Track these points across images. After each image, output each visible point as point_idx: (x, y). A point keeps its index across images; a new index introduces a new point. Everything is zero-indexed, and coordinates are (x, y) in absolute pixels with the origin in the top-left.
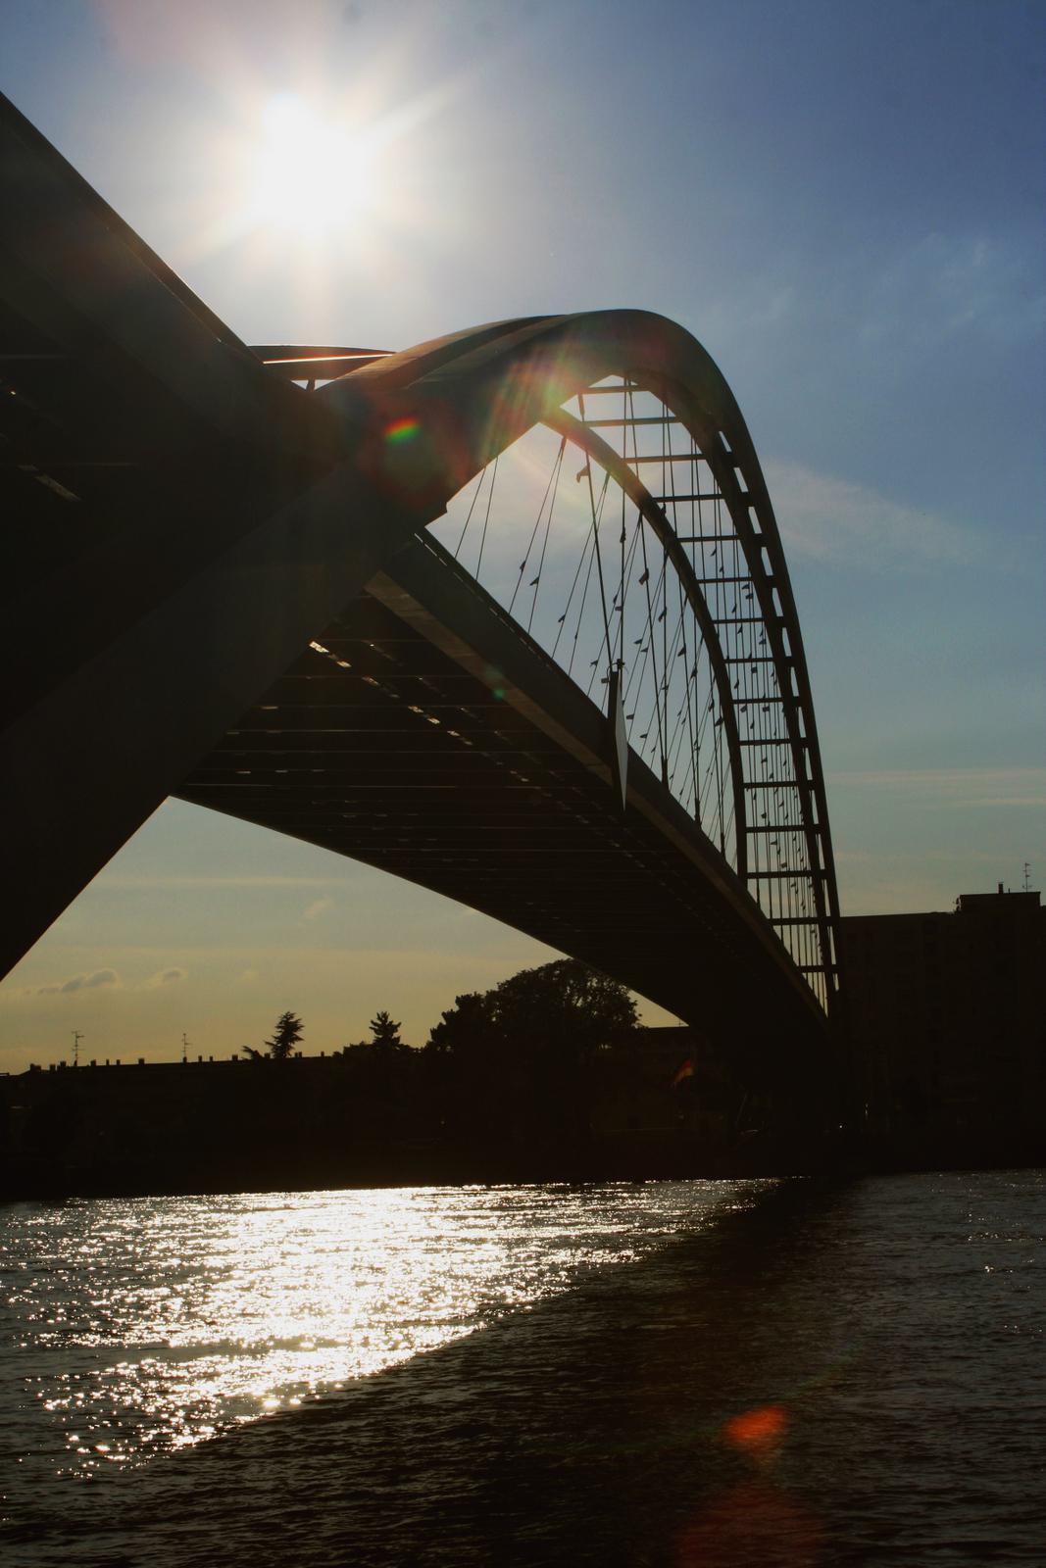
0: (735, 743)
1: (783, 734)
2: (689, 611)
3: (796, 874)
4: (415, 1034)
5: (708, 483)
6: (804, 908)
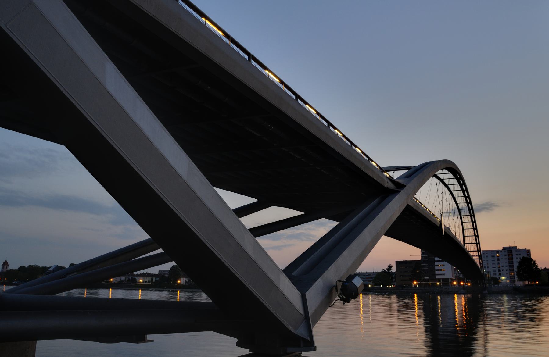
2: (450, 195)
4: (518, 248)
6: (470, 240)
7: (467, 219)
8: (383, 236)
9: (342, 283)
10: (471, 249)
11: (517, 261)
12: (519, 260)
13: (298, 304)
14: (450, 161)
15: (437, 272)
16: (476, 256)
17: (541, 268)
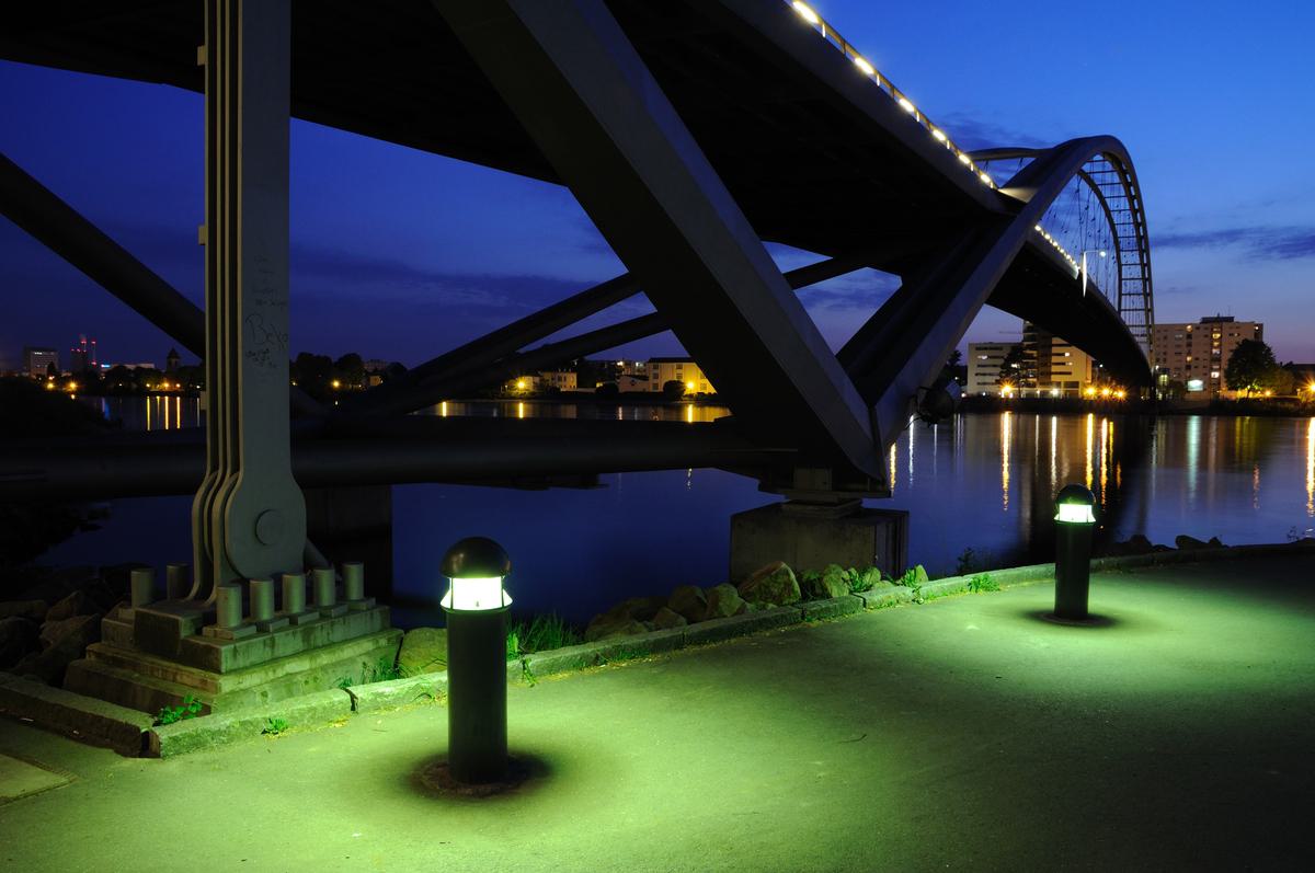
0: (1120, 266)
1: (1138, 262)
5: (1116, 179)
7: (1130, 257)
9: (925, 391)
12: (1234, 347)
14: (1109, 136)
15: (1054, 369)
16: (1142, 335)
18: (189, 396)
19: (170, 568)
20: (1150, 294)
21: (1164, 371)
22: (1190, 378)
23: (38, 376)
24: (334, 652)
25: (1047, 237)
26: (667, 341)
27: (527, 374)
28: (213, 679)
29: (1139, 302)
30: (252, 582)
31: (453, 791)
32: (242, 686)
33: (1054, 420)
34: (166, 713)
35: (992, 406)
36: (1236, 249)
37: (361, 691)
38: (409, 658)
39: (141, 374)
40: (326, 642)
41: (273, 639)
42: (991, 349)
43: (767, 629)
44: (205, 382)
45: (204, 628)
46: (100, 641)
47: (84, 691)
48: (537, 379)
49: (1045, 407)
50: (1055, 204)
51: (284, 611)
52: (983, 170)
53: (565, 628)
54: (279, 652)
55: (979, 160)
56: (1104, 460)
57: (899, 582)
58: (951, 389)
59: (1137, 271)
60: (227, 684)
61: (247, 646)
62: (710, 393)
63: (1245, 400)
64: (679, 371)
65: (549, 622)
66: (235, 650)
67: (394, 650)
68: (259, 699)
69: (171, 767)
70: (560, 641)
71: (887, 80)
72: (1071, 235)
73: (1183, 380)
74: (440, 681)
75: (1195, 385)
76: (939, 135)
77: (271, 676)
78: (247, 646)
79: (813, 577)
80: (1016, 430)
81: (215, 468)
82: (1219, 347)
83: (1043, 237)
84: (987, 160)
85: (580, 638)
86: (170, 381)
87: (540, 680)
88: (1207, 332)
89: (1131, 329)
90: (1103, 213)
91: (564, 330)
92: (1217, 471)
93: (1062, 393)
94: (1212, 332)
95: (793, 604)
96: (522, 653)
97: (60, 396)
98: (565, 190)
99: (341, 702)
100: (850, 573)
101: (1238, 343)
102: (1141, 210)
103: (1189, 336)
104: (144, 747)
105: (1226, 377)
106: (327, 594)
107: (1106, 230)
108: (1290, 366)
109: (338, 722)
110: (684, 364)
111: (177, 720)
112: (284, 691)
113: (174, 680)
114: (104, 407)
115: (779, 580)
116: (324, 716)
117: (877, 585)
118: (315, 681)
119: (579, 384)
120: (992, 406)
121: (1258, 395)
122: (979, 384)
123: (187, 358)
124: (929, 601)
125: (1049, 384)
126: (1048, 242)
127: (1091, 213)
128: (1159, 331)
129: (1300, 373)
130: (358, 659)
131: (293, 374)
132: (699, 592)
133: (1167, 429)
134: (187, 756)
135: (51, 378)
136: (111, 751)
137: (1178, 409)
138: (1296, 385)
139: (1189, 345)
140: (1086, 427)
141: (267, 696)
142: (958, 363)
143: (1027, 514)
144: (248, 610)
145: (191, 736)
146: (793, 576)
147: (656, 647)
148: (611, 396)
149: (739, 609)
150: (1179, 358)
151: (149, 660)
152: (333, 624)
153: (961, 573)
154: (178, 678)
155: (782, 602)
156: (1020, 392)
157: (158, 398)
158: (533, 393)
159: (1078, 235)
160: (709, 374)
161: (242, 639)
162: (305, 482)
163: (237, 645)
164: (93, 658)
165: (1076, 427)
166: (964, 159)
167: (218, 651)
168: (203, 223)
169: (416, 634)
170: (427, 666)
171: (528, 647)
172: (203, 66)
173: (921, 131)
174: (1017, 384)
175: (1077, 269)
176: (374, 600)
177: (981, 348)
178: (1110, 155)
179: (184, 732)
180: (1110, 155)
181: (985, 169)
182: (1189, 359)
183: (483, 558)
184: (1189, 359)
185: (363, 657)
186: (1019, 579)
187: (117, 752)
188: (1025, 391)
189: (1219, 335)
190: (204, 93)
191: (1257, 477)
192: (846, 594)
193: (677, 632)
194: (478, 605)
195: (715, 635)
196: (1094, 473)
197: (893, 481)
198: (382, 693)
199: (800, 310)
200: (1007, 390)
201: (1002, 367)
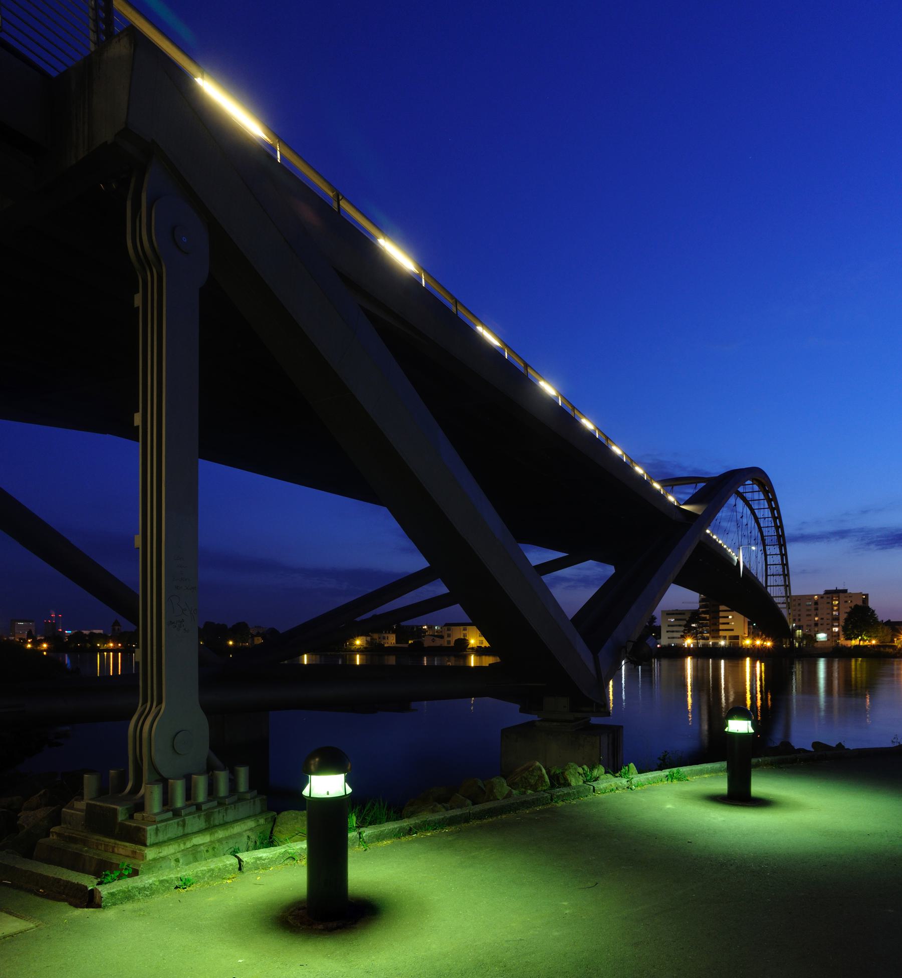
0: (766, 556)
1: (778, 553)
3: (780, 586)
5: (762, 497)
7: (773, 550)
8: (672, 584)
9: (632, 643)
10: (775, 594)
11: (846, 611)
12: (848, 610)
13: (591, 666)
16: (783, 603)
17: (882, 621)
18: (127, 652)
19: (112, 772)
20: (788, 575)
21: (799, 627)
22: (818, 632)
23: (20, 639)
24: (227, 829)
25: (715, 537)
26: (456, 611)
27: (361, 635)
28: (141, 850)
29: (780, 580)
30: (170, 781)
31: (310, 927)
32: (161, 855)
33: (723, 662)
34: (107, 875)
35: (680, 653)
36: (845, 544)
37: (246, 857)
38: (280, 832)
39: (93, 637)
40: (222, 822)
41: (184, 821)
42: (677, 614)
43: (528, 808)
44: (138, 642)
45: (135, 814)
46: (60, 824)
47: (49, 861)
48: (369, 638)
49: (716, 653)
50: (719, 514)
51: (192, 801)
52: (669, 493)
53: (389, 809)
54: (189, 830)
55: (667, 486)
56: (758, 689)
57: (617, 775)
58: (650, 642)
59: (778, 559)
60: (151, 854)
61: (166, 826)
62: (485, 647)
63: (856, 647)
64: (465, 632)
65: (377, 805)
66: (157, 830)
67: (269, 826)
68: (173, 863)
69: (109, 914)
70: (385, 818)
71: (604, 434)
72: (731, 536)
73: (813, 634)
74: (302, 848)
75: (822, 636)
76: (639, 470)
77: (182, 847)
78: (166, 826)
79: (558, 772)
80: (696, 669)
81: (145, 701)
82: (838, 610)
83: (712, 537)
84: (672, 486)
85: (399, 815)
86: (113, 642)
87: (371, 846)
88: (829, 600)
89: (775, 599)
90: (753, 521)
91: (392, 602)
92: (839, 695)
93: (727, 643)
94: (833, 600)
95: (544, 791)
96: (358, 827)
97: (35, 652)
98: (384, 510)
99: (231, 865)
100: (583, 769)
101: (851, 607)
102: (780, 517)
103: (816, 603)
104: (90, 900)
105: (843, 631)
106: (223, 788)
107: (756, 532)
108: (889, 623)
109: (229, 879)
110: (468, 627)
111: (114, 880)
112: (191, 858)
113: (113, 852)
114: (67, 660)
115: (534, 774)
116: (220, 875)
117: (602, 777)
118: (213, 850)
119: (397, 642)
120: (680, 653)
121: (867, 643)
122: (669, 638)
123: (126, 626)
124: (639, 788)
125: (719, 637)
126: (715, 540)
127: (745, 521)
128: (795, 600)
129: (894, 627)
130: (244, 833)
131: (201, 637)
132: (480, 783)
133: (802, 667)
134: (121, 907)
135: (29, 641)
136: (66, 903)
137: (811, 653)
138: (894, 636)
139: (816, 609)
140: (745, 666)
141: (179, 861)
142: (655, 624)
143: (705, 727)
144: (167, 801)
145: (124, 892)
146: (544, 771)
147: (450, 822)
148: (419, 649)
149: (508, 794)
150: (809, 618)
151: (96, 838)
152: (226, 810)
153: (660, 768)
154: (116, 850)
155: (536, 788)
156: (698, 643)
157: (105, 653)
158: (366, 648)
159: (736, 535)
160: (484, 634)
161: (162, 821)
162: (207, 709)
163: (159, 825)
164: (55, 837)
165: (738, 667)
166: (657, 486)
167: (144, 830)
168: (138, 534)
169: (285, 814)
170: (292, 839)
171: (362, 823)
172: (138, 427)
173: (627, 468)
174: (695, 638)
175: (736, 558)
176: (256, 791)
177: (670, 614)
178: (757, 480)
179: (119, 889)
180: (757, 480)
181: (671, 492)
182: (816, 619)
183: (330, 764)
184: (816, 619)
185: (248, 832)
186: (701, 772)
187: (71, 904)
188: (701, 642)
189: (837, 602)
190: (139, 442)
191: (868, 700)
192: (581, 783)
193: (465, 811)
194: (328, 794)
195: (492, 812)
196: (751, 698)
197: (611, 705)
198: (261, 857)
199: (546, 590)
200: (689, 642)
201: (685, 626)
